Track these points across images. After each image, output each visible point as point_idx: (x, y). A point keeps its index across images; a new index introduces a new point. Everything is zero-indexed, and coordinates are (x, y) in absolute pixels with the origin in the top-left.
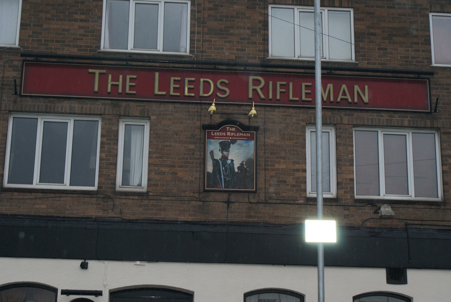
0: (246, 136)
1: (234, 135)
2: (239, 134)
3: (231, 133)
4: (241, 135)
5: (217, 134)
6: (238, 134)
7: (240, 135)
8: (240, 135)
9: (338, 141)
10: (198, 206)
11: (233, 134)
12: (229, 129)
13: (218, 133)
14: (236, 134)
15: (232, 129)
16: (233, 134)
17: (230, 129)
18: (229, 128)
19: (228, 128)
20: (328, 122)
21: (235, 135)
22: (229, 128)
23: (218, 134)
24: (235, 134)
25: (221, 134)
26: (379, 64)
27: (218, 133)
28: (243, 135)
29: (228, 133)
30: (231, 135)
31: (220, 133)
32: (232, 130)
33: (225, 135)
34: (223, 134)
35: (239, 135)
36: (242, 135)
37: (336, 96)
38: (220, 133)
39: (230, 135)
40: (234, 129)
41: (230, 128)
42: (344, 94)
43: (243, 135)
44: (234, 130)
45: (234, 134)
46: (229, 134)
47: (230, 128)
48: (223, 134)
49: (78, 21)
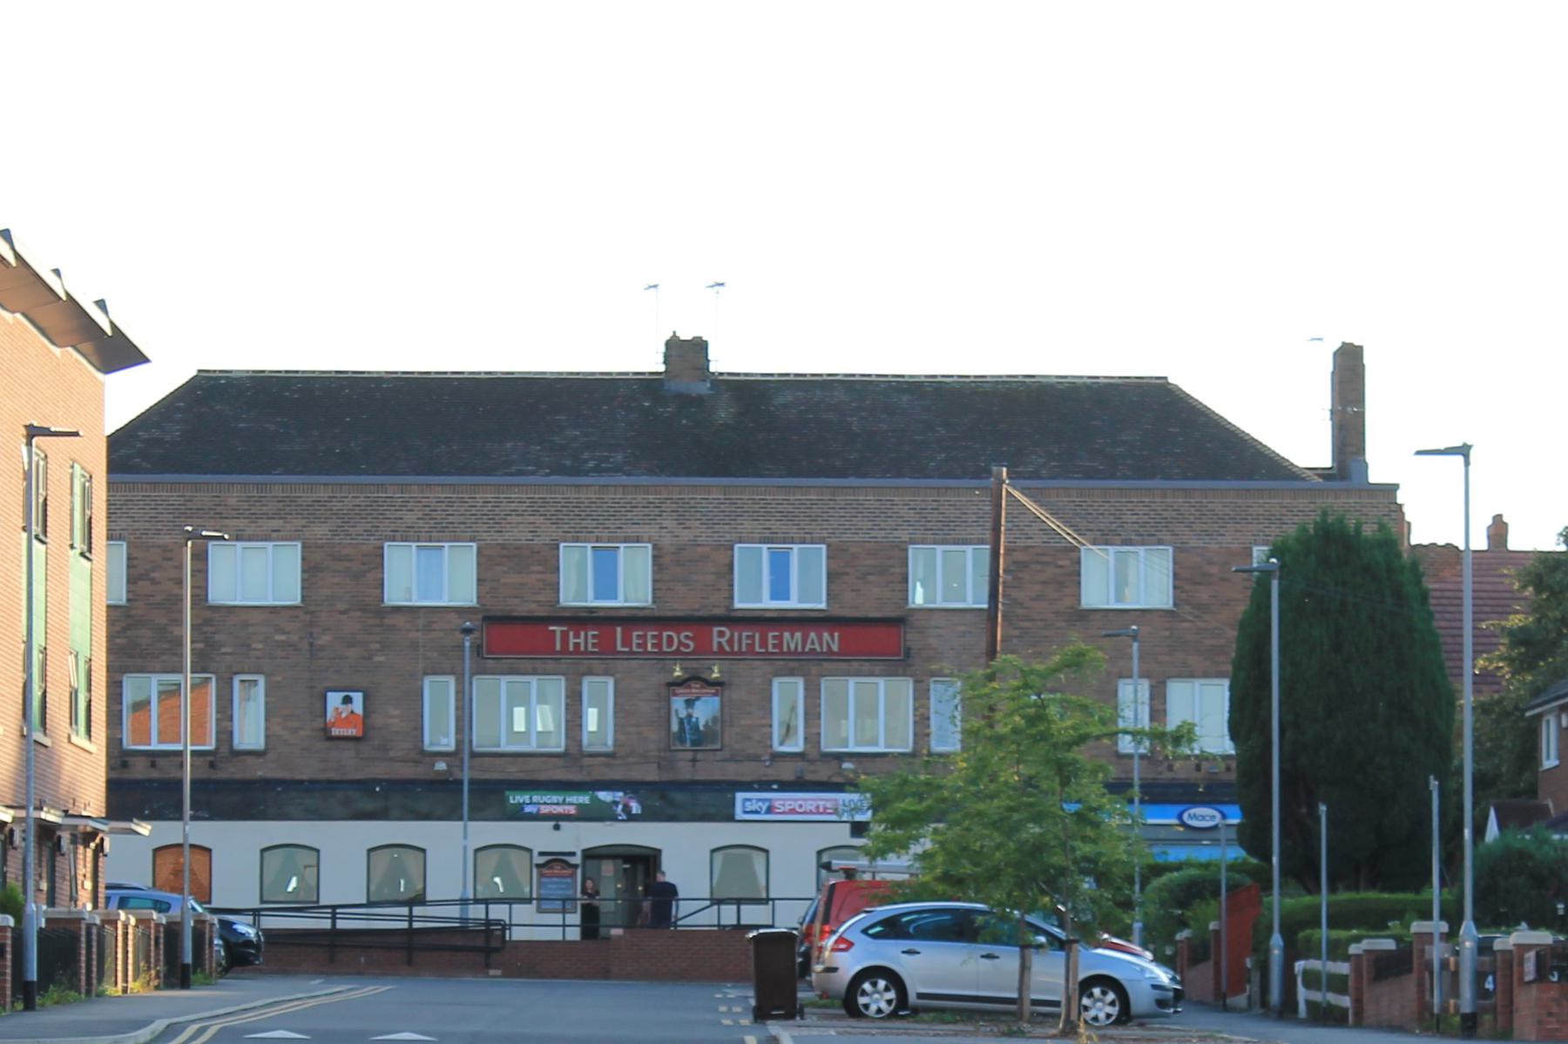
6: (771, 641)
11: (745, 642)
12: (565, 636)
15: (581, 640)
17: (572, 641)
18: (565, 629)
21: (757, 649)
22: (565, 629)
25: (670, 639)
41: (571, 634)
42: (813, 643)
47: (571, 634)
48: (680, 643)
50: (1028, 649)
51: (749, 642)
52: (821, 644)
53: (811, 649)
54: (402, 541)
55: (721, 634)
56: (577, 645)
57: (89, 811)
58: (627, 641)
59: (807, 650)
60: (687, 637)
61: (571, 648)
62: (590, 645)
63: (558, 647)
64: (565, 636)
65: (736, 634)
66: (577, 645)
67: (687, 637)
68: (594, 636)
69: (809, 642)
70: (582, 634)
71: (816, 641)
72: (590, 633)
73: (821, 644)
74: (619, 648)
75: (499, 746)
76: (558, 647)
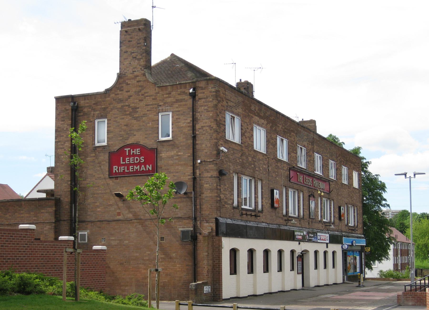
0: (145, 170)
1: (124, 171)
2: (134, 167)
3: (120, 167)
4: (137, 170)
5: (130, 161)
6: (131, 169)
7: (135, 171)
8: (135, 171)
9: (360, 183)
10: (188, 157)
11: (122, 169)
12: (129, 151)
13: (131, 158)
14: (128, 169)
15: (135, 152)
16: (122, 169)
17: (132, 152)
18: (129, 149)
19: (127, 150)
20: (262, 114)
21: (126, 171)
22: (129, 149)
23: (131, 160)
24: (126, 167)
25: (137, 160)
26: (43, 213)
27: (131, 158)
28: (140, 168)
29: (114, 167)
30: (120, 172)
31: (134, 159)
32: (135, 154)
33: (143, 160)
34: (140, 160)
35: (133, 170)
36: (139, 170)
37: (140, 169)
38: (136, 158)
39: (117, 172)
40: (137, 151)
41: (132, 150)
42: (143, 168)
43: (140, 168)
44: (137, 154)
45: (125, 168)
46: (116, 169)
47: (132, 150)
48: (140, 160)
49: (116, 240)
50: (362, 175)
51: (124, 169)
52: (146, 168)
53: (142, 170)
54: (107, 130)
55: (115, 168)
56: (133, 153)
57: (400, 285)
58: (124, 160)
59: (141, 170)
60: (142, 158)
61: (132, 154)
62: (137, 152)
63: (127, 154)
64: (129, 151)
65: (120, 167)
66: (133, 153)
67: (142, 158)
68: (138, 150)
69: (142, 167)
70: (135, 150)
71: (144, 167)
72: (137, 149)
73: (146, 168)
74: (122, 163)
75: (293, 191)
76: (127, 154)
